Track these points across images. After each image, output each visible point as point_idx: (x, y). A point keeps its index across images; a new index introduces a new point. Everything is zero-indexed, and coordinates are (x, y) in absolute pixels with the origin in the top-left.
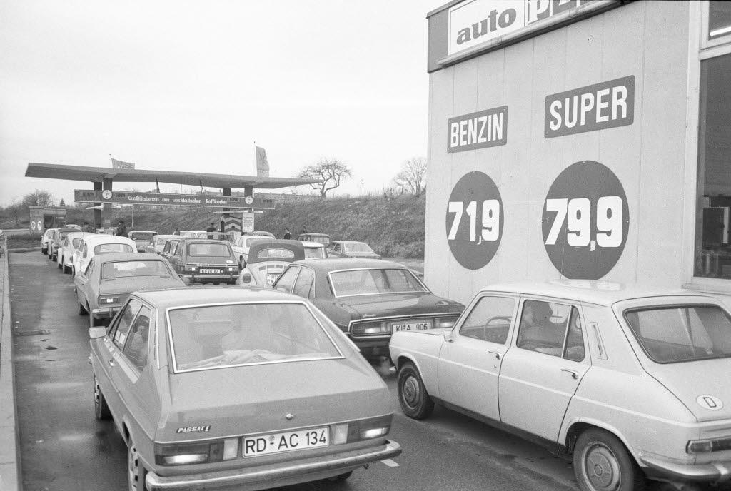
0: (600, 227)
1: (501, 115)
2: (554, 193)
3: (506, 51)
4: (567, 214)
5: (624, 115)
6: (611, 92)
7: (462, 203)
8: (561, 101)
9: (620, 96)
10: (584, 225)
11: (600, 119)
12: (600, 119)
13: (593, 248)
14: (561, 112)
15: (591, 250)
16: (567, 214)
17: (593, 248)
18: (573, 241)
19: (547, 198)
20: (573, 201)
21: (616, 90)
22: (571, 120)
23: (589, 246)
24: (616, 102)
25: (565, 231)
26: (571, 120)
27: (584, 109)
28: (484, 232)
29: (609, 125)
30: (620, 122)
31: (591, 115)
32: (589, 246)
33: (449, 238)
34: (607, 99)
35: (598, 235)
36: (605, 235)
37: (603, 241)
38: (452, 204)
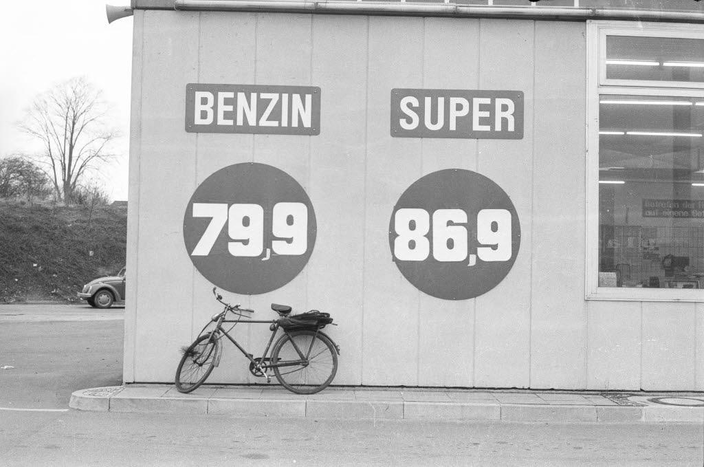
0: (482, 239)
1: (309, 97)
2: (407, 201)
3: (537, 26)
4: (228, 220)
5: (511, 128)
6: (493, 102)
7: (227, 205)
8: (469, 100)
9: (505, 108)
10: (255, 233)
11: (476, 127)
12: (476, 127)
13: (472, 262)
14: (420, 111)
15: (469, 265)
16: (228, 220)
17: (472, 262)
18: (235, 250)
19: (396, 209)
20: (235, 206)
21: (499, 102)
22: (434, 121)
23: (467, 260)
24: (499, 115)
25: (224, 238)
26: (434, 121)
27: (454, 114)
28: (275, 244)
29: (492, 135)
30: (504, 135)
31: (465, 122)
32: (467, 260)
33: (196, 253)
34: (490, 108)
35: (274, 242)
36: (241, 244)
37: (486, 255)
38: (196, 206)
